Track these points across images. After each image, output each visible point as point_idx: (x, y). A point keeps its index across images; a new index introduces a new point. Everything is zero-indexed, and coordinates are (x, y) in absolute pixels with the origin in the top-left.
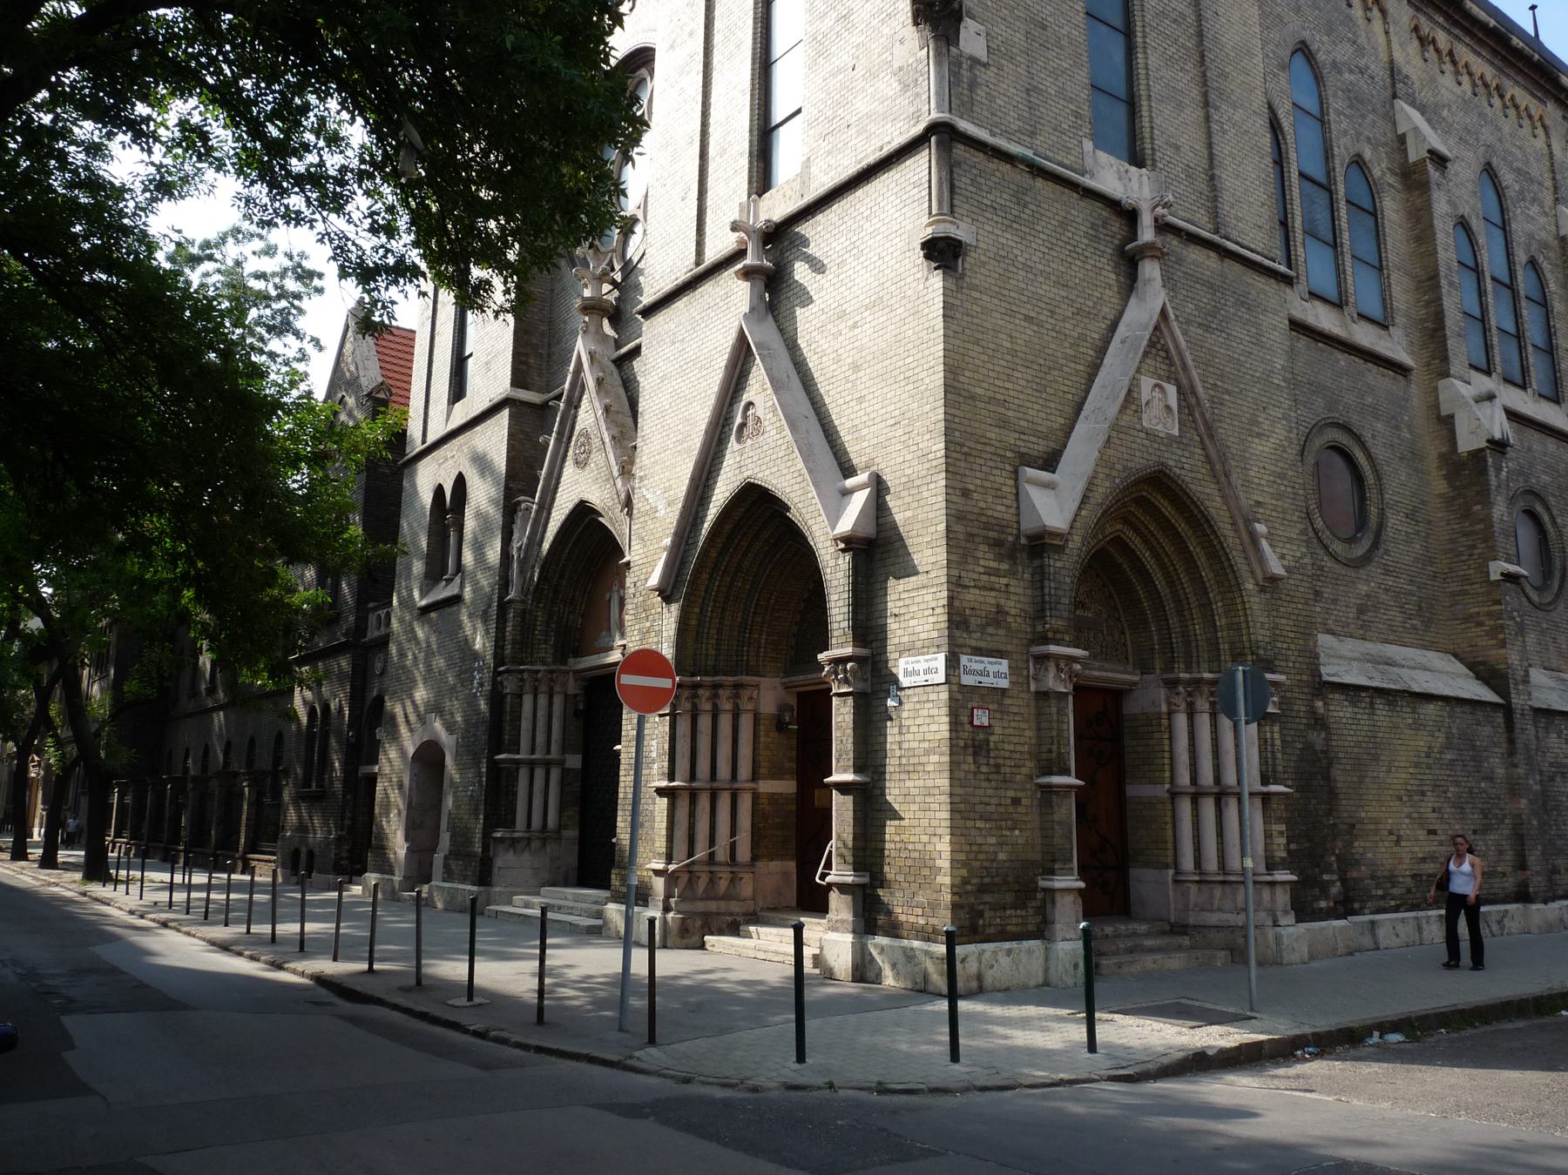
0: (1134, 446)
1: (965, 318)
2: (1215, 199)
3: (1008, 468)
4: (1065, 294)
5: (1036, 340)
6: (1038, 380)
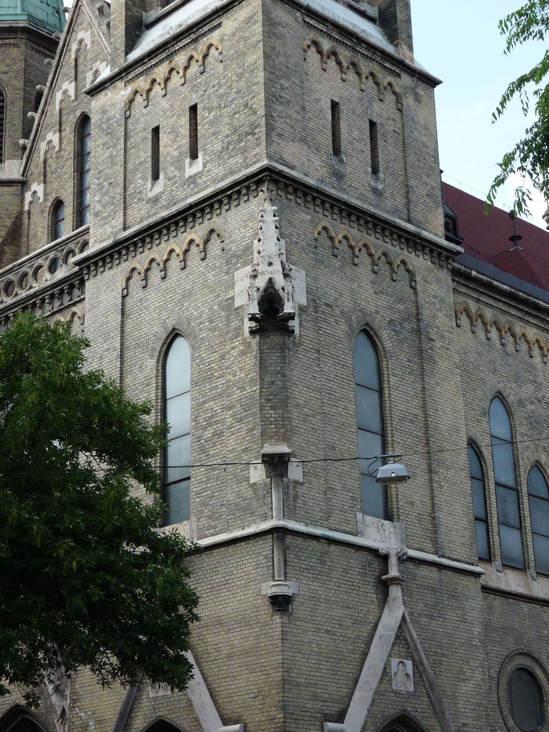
0: (388, 702)
1: (293, 638)
2: (436, 532)
3: (318, 723)
4: (347, 612)
5: (332, 644)
6: (333, 668)
